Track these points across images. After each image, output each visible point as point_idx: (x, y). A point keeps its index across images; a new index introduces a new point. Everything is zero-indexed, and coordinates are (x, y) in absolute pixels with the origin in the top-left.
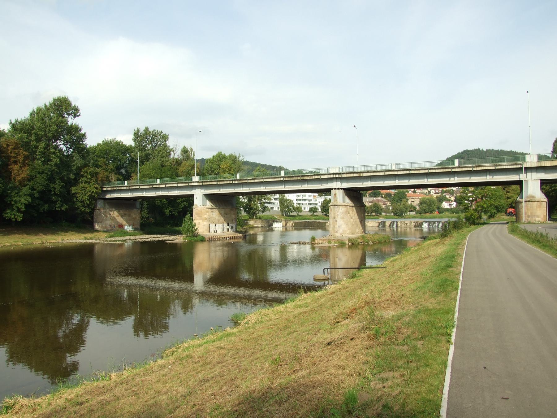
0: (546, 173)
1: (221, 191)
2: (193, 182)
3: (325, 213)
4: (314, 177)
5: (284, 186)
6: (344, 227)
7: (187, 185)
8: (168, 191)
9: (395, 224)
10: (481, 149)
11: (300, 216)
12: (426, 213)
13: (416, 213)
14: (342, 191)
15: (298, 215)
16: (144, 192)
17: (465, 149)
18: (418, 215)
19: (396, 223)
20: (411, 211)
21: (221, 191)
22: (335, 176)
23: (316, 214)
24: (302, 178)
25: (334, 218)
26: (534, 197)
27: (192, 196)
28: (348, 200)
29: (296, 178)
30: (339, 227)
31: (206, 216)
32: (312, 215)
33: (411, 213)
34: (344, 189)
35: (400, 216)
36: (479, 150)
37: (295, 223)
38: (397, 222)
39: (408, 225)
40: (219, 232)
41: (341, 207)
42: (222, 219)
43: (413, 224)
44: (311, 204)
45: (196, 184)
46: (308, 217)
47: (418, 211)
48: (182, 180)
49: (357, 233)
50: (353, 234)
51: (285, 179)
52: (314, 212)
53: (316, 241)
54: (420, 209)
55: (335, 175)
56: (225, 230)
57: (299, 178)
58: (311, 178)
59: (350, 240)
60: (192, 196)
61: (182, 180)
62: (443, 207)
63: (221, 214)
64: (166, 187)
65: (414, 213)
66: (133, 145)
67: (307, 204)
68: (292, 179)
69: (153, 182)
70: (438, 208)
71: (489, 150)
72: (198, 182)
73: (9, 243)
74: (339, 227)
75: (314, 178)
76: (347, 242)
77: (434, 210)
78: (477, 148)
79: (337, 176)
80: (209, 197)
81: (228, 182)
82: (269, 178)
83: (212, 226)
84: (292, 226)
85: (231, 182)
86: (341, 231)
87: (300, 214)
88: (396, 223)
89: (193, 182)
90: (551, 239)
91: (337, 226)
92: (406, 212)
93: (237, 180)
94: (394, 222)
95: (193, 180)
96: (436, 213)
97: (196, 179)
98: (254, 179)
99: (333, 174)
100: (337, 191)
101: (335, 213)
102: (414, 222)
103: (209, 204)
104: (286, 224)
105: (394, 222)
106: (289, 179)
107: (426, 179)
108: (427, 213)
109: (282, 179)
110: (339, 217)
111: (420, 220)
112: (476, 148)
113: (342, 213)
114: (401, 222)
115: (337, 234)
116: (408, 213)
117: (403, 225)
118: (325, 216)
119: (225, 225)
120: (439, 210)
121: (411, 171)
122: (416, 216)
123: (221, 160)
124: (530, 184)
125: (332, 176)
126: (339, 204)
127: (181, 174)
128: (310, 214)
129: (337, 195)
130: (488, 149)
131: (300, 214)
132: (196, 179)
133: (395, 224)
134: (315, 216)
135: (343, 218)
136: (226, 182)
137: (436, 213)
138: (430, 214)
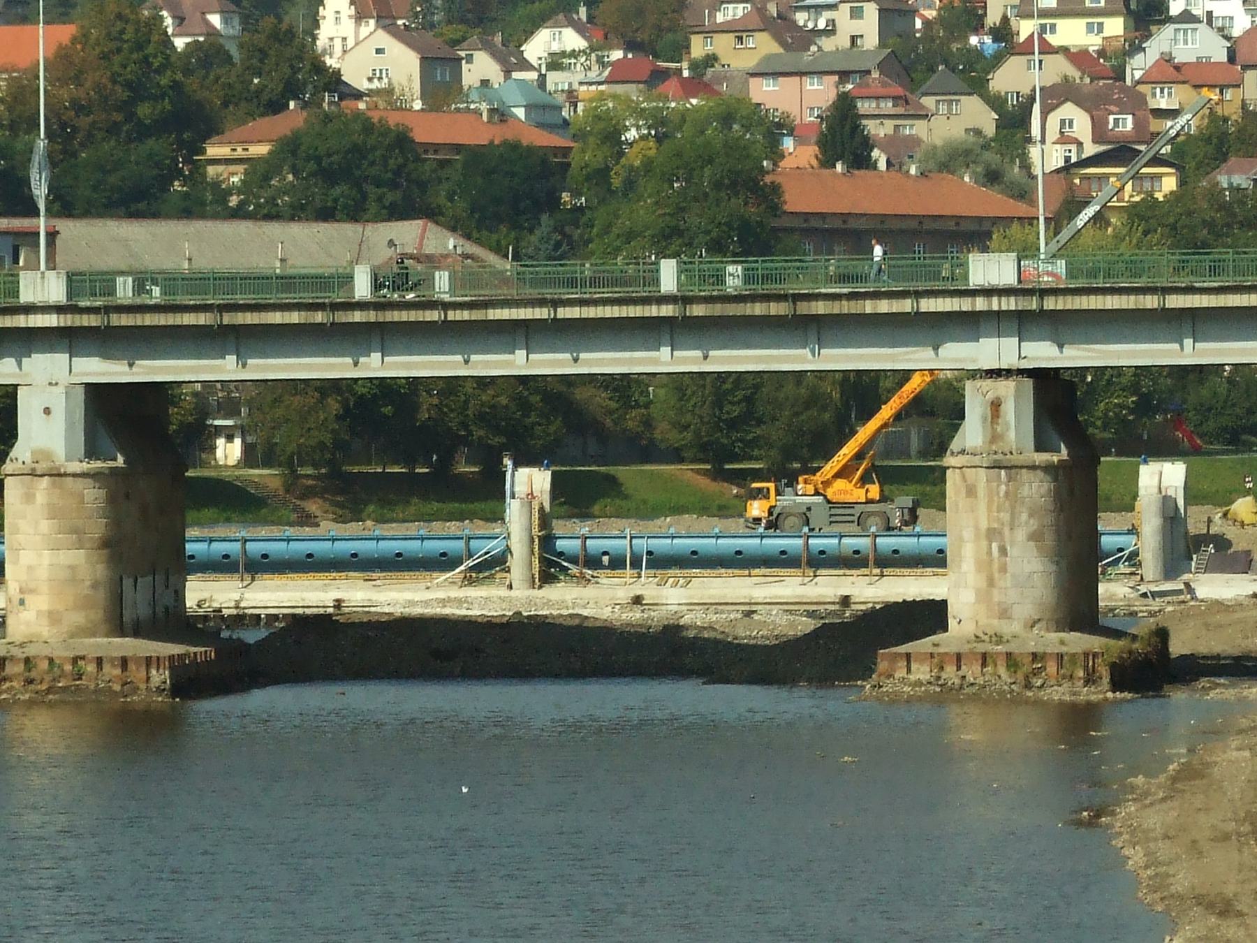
0: (106, 356)
1: (367, 367)
2: (29, 309)
4: (869, 307)
7: (1151, 302)
8: (466, 351)
21: (367, 367)
22: (995, 304)
45: (51, 320)
48: (1214, 271)
55: (995, 300)
61: (936, 276)
66: (179, 50)
72: (59, 309)
75: (868, 310)
79: (1009, 304)
81: (295, 317)
85: (319, 317)
89: (29, 309)
90: (45, 665)
93: (362, 306)
95: (26, 297)
98: (485, 305)
107: (521, 354)
109: (667, 310)
121: (31, 317)
125: (980, 304)
136: (277, 318)
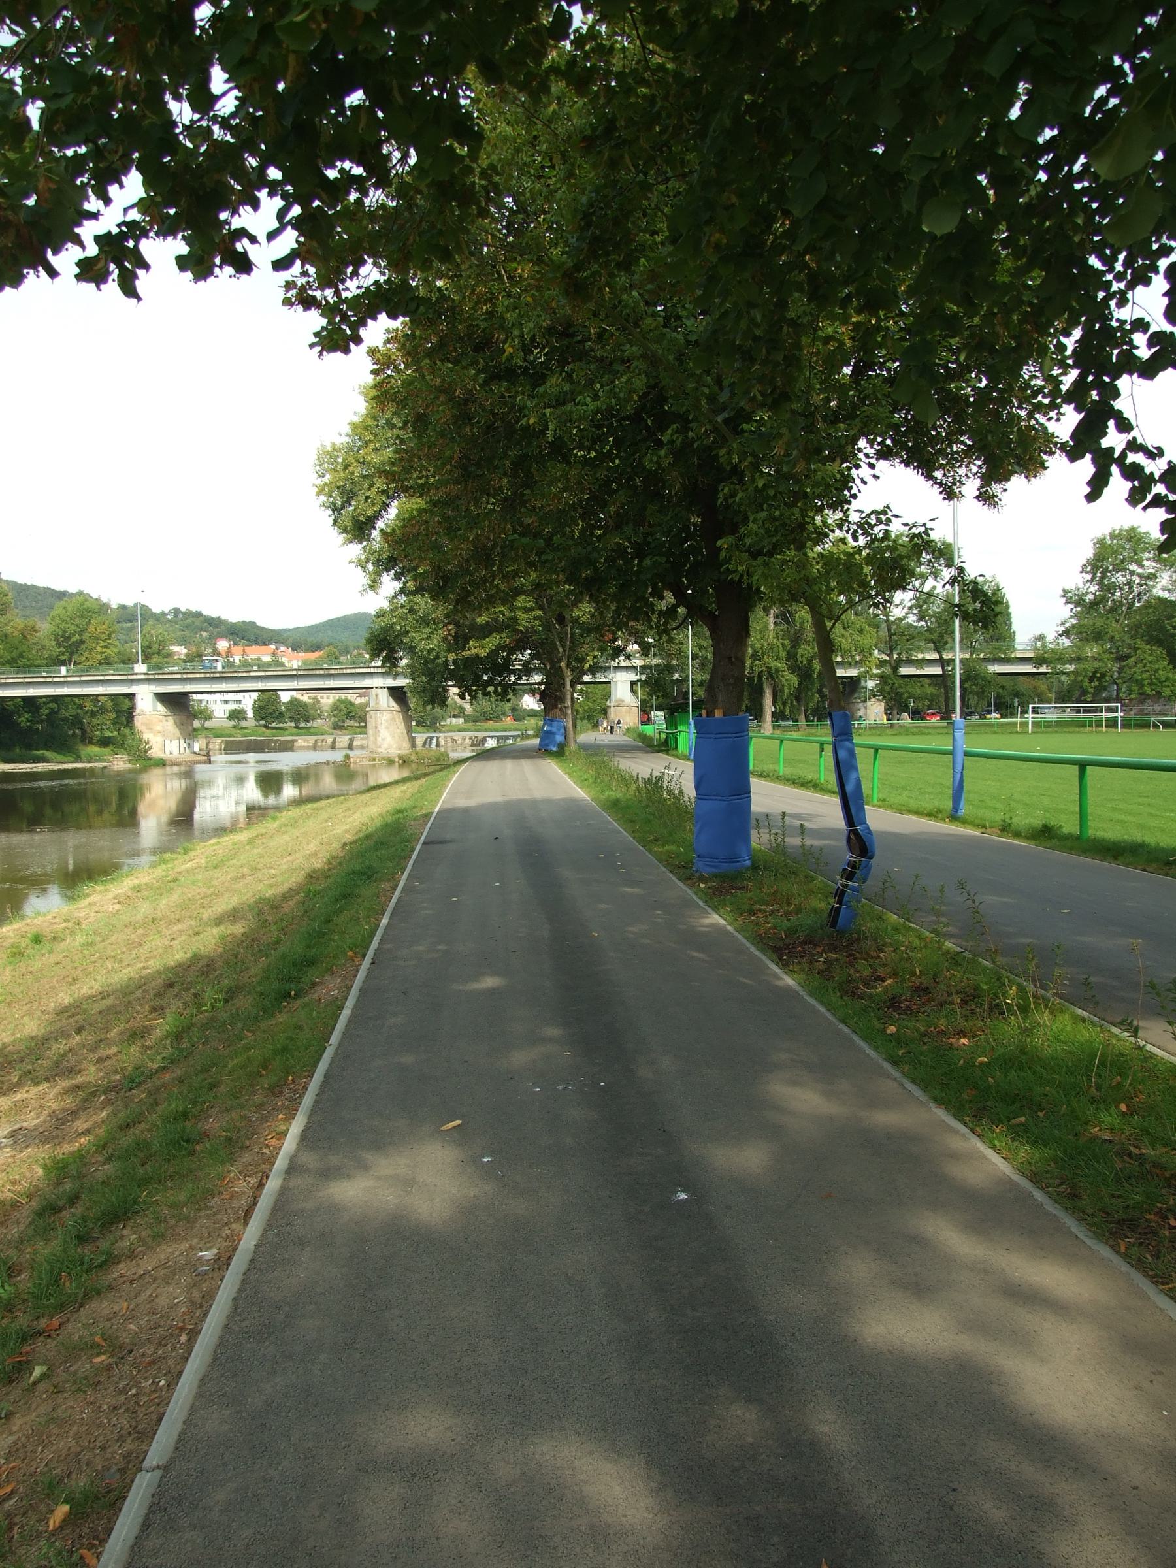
2: (136, 674)
3: (263, 722)
4: (345, 671)
6: (389, 739)
9: (434, 742)
11: (207, 729)
12: (488, 719)
13: (465, 722)
14: (386, 690)
15: (203, 726)
18: (469, 725)
19: (435, 739)
20: (454, 716)
23: (243, 724)
24: (326, 672)
25: (376, 727)
26: (623, 701)
27: (131, 697)
28: (393, 703)
29: (318, 672)
30: (383, 740)
31: (159, 728)
32: (234, 727)
33: (454, 720)
34: (388, 688)
35: (430, 727)
37: (227, 743)
38: (438, 738)
39: (459, 742)
40: (176, 753)
41: (385, 713)
42: (177, 732)
43: (467, 740)
44: (226, 702)
45: (143, 677)
46: (227, 732)
47: (468, 716)
49: (405, 749)
50: (400, 749)
51: (299, 673)
52: (239, 720)
53: (352, 760)
54: (474, 710)
56: (182, 750)
57: (322, 672)
58: (341, 672)
59: (400, 757)
60: (131, 697)
62: (525, 706)
63: (176, 723)
65: (461, 720)
67: (219, 702)
68: (311, 672)
69: (55, 672)
70: (514, 709)
74: (383, 740)
76: (397, 759)
77: (504, 714)
80: (162, 697)
83: (167, 742)
84: (221, 750)
86: (385, 746)
87: (208, 724)
88: (435, 739)
89: (136, 674)
91: (379, 739)
92: (443, 718)
94: (431, 738)
95: (136, 671)
96: (509, 720)
97: (140, 668)
100: (379, 691)
101: (376, 721)
102: (471, 738)
103: (161, 708)
104: (208, 745)
105: (431, 738)
106: (306, 673)
108: (490, 719)
110: (383, 726)
111: (481, 735)
113: (387, 721)
114: (445, 737)
115: (380, 750)
116: (448, 721)
117: (450, 744)
118: (264, 729)
119: (182, 741)
120: (516, 713)
122: (465, 726)
123: (98, 613)
124: (619, 685)
126: (382, 708)
128: (232, 723)
129: (380, 696)
131: (208, 724)
132: (140, 668)
133: (434, 742)
134: (242, 728)
135: (387, 728)
137: (509, 720)
138: (496, 722)
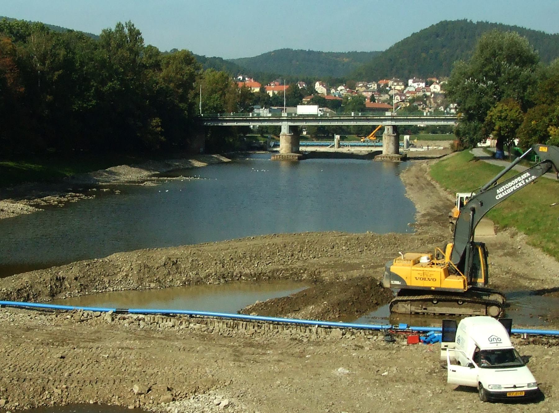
5: (236, 123)
10: (468, 21)
16: (320, 122)
17: (443, 20)
22: (388, 118)
27: (281, 126)
36: (465, 20)
45: (285, 118)
58: (373, 118)
60: (281, 126)
64: (407, 119)
71: (482, 22)
73: (531, 164)
78: (463, 19)
79: (390, 118)
82: (237, 117)
93: (319, 117)
99: (388, 116)
112: (461, 18)
127: (498, 70)
130: (480, 21)
136: (310, 118)
